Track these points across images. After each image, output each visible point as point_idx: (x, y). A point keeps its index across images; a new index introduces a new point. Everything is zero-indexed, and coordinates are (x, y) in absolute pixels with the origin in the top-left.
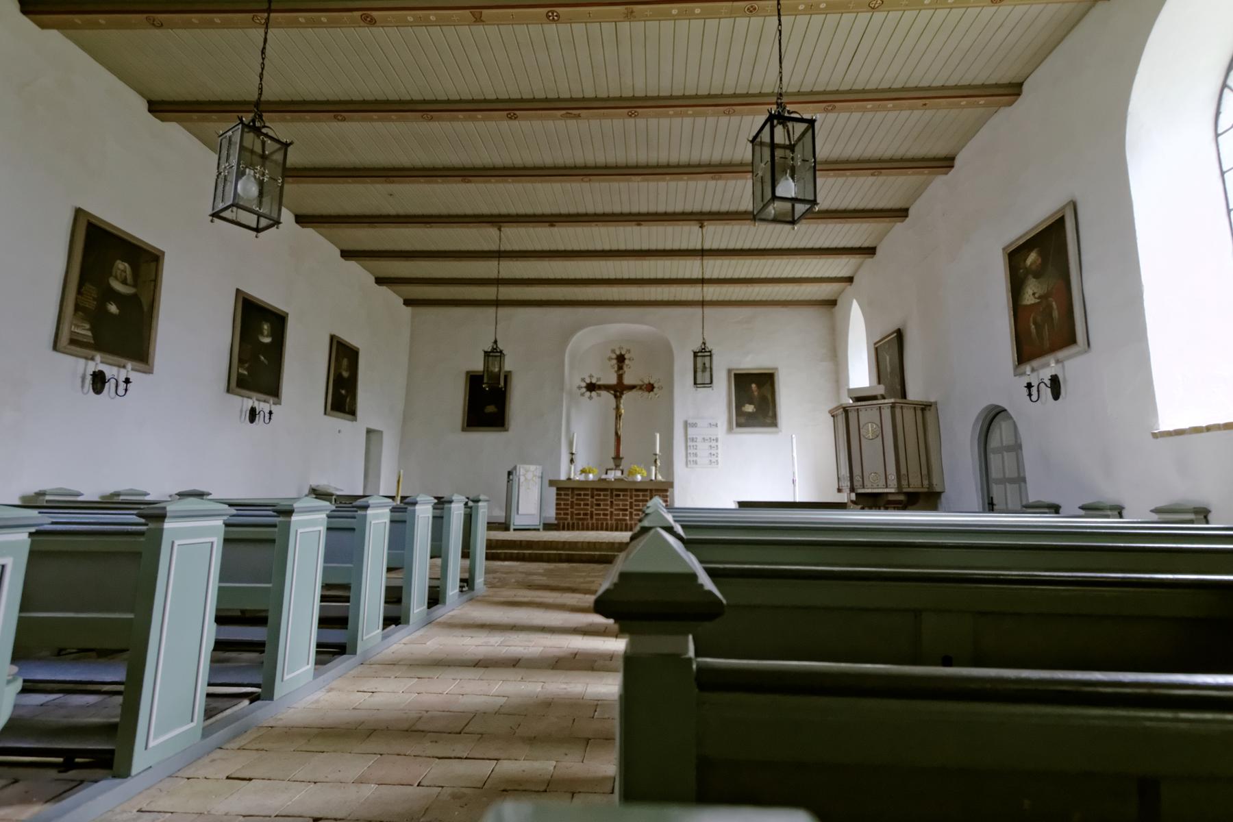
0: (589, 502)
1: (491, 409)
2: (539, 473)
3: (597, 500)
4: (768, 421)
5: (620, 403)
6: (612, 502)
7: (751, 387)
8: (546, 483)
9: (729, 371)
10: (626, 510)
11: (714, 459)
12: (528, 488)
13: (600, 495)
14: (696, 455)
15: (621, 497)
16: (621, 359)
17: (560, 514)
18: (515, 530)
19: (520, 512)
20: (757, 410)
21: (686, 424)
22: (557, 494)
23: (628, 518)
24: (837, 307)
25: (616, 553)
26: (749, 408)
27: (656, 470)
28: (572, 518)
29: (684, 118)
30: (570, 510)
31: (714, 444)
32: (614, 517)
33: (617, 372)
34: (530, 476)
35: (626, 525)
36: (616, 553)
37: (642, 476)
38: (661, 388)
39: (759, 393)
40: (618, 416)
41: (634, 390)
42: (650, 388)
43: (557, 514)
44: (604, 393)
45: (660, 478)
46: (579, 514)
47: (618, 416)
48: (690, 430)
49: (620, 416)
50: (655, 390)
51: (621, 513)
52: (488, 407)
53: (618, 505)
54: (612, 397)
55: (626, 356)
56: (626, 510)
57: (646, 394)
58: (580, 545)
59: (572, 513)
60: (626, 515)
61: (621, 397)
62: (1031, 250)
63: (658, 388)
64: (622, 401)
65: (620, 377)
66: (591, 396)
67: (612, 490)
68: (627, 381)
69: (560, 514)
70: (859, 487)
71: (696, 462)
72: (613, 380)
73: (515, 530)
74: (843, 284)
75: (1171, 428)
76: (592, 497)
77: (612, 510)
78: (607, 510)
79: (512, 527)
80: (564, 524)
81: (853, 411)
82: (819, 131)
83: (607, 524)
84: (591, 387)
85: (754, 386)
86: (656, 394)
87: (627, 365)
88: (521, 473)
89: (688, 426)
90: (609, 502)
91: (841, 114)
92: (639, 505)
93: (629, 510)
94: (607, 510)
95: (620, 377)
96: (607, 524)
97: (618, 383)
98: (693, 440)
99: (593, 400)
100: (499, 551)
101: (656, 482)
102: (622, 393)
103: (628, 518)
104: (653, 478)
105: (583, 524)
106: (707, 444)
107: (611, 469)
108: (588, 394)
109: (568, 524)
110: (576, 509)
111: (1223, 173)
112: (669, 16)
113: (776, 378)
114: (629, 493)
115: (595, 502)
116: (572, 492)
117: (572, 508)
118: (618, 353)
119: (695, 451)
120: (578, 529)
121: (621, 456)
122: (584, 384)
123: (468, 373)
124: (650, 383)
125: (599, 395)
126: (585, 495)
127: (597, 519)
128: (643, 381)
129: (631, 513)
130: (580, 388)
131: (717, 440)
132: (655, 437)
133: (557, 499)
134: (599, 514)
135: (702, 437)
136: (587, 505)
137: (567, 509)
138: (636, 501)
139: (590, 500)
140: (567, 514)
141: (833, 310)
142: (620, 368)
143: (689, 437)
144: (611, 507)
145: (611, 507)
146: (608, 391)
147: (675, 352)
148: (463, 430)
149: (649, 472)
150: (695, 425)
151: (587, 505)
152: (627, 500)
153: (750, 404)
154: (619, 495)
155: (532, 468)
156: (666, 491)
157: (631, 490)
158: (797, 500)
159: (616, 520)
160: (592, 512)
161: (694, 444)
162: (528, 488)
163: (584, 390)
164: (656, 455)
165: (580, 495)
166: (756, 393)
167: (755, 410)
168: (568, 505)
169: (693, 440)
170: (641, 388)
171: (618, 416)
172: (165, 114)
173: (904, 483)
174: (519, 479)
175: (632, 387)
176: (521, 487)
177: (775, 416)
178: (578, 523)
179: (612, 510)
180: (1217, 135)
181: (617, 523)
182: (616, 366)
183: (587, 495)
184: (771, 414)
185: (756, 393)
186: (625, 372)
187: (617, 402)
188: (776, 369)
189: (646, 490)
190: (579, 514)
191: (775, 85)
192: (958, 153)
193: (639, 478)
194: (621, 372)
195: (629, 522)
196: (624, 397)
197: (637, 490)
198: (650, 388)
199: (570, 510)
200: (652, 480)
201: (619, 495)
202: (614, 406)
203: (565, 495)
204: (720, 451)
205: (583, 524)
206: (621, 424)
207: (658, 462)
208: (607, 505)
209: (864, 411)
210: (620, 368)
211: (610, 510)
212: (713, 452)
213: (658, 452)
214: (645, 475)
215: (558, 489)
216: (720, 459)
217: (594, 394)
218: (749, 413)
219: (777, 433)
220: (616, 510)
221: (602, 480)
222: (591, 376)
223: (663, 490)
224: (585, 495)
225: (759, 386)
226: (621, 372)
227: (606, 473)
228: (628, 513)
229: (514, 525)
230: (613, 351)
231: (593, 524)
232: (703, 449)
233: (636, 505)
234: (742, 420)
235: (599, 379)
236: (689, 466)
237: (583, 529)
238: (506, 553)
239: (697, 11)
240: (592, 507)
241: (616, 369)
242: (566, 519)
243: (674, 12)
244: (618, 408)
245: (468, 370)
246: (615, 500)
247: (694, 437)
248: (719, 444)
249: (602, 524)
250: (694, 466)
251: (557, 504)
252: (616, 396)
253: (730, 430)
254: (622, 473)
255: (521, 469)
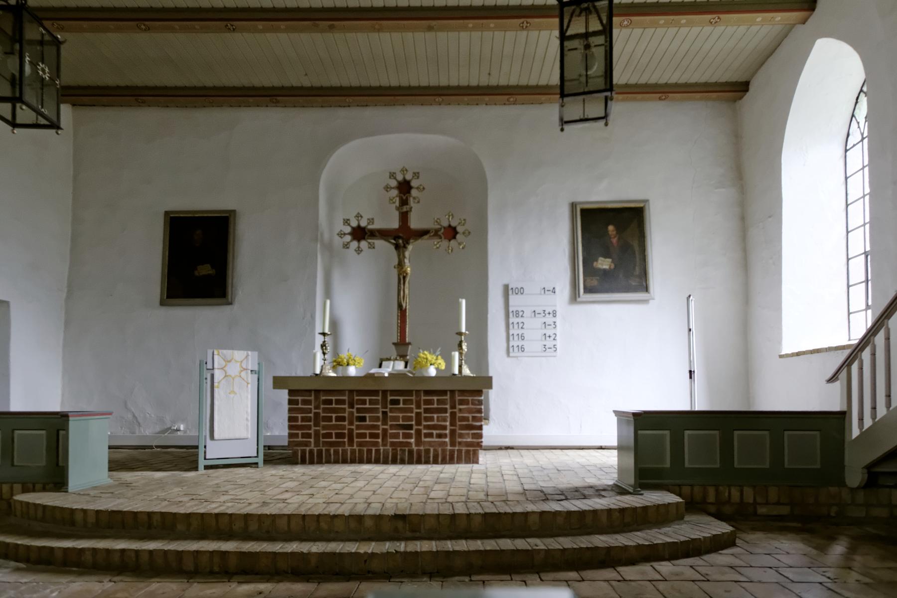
0: (346, 415)
1: (205, 270)
2: (252, 364)
3: (359, 410)
4: (634, 283)
5: (404, 257)
6: (385, 413)
7: (607, 231)
8: (268, 383)
9: (573, 206)
10: (410, 427)
11: (549, 343)
12: (233, 392)
13: (364, 402)
14: (522, 337)
15: (401, 405)
16: (405, 187)
17: (296, 435)
18: (207, 467)
19: (216, 436)
20: (616, 266)
21: (506, 289)
22: (290, 402)
23: (413, 440)
26: (604, 264)
27: (460, 360)
28: (317, 444)
29: (484, 32)
30: (313, 428)
31: (549, 319)
32: (390, 440)
33: (397, 209)
34: (233, 369)
35: (411, 452)
37: (437, 369)
38: (467, 233)
39: (619, 239)
40: (402, 277)
41: (426, 237)
42: (451, 233)
43: (291, 435)
44: (379, 243)
45: (466, 371)
46: (329, 435)
47: (402, 277)
48: (513, 299)
49: (404, 278)
50: (458, 236)
51: (401, 432)
52: (200, 267)
53: (396, 419)
54: (393, 247)
55: (414, 183)
56: (410, 427)
57: (445, 243)
58: (282, 524)
59: (317, 433)
60: (409, 436)
61: (405, 247)
63: (464, 233)
64: (407, 254)
65: (404, 217)
66: (359, 247)
67: (385, 392)
68: (415, 223)
69: (296, 435)
71: (522, 349)
72: (395, 224)
73: (207, 467)
75: (789, 352)
76: (351, 406)
77: (385, 427)
78: (377, 427)
79: (202, 463)
80: (304, 452)
82: (616, 42)
83: (378, 451)
84: (360, 234)
85: (611, 228)
86: (460, 244)
87: (414, 198)
88: (216, 366)
89: (510, 292)
90: (380, 415)
91: (635, 30)
92: (432, 419)
93: (415, 427)
94: (377, 427)
95: (404, 217)
96: (378, 451)
97: (400, 226)
98: (517, 314)
99: (363, 254)
100: (299, 455)
101: (461, 377)
102: (406, 242)
103: (413, 440)
104: (456, 371)
105: (336, 452)
106: (539, 321)
107: (389, 359)
108: (355, 244)
109: (311, 452)
110: (324, 428)
112: (465, 28)
114: (448, 397)
115: (356, 415)
116: (317, 398)
117: (316, 425)
118: (400, 177)
119: (520, 332)
120: (328, 462)
121: (407, 340)
122: (348, 229)
123: (167, 213)
124: (450, 226)
125: (372, 246)
126: (338, 402)
127: (360, 444)
128: (439, 224)
129: (418, 432)
130: (341, 234)
131: (554, 314)
132: (459, 306)
133: (290, 410)
134: (363, 436)
135: (533, 309)
136: (343, 419)
137: (309, 428)
138: (427, 411)
139: (348, 410)
140: (309, 436)
142: (404, 202)
143: (511, 309)
144: (385, 422)
145: (385, 422)
146: (386, 240)
147: (489, 186)
148: (162, 303)
149: (449, 361)
150: (520, 291)
151: (343, 419)
152: (411, 410)
153: (606, 257)
154: (396, 402)
155: (239, 355)
156: (479, 392)
157: (418, 392)
159: (392, 444)
160: (351, 432)
161: (520, 320)
162: (233, 392)
163: (348, 238)
164: (460, 334)
165: (330, 402)
166: (615, 241)
167: (613, 266)
168: (309, 419)
169: (517, 314)
170: (436, 234)
171: (402, 277)
172: (82, 98)
174: (212, 376)
175: (422, 234)
176: (216, 390)
177: (644, 274)
178: (328, 451)
179: (385, 427)
181: (394, 450)
182: (398, 199)
183: (342, 402)
184: (637, 271)
185: (615, 241)
186: (411, 208)
187: (399, 256)
188: (646, 201)
189: (444, 393)
190: (329, 435)
191: (556, 56)
193: (432, 372)
194: (405, 209)
195: (414, 448)
196: (410, 247)
197: (428, 392)
198: (451, 233)
199: (313, 428)
200: (454, 375)
201: (396, 402)
202: (396, 262)
203: (305, 402)
204: (558, 331)
205: (336, 452)
206: (407, 291)
207: (464, 347)
208: (377, 419)
210: (404, 202)
211: (415, 411)
212: (549, 332)
213: (463, 330)
214: (443, 367)
215: (291, 392)
216: (558, 343)
217: (364, 244)
218: (605, 270)
219: (646, 301)
220: (392, 427)
221: (370, 377)
222: (359, 216)
224: (338, 402)
225: (620, 230)
226: (405, 209)
227: (380, 366)
228: (413, 432)
229: (205, 459)
230: (392, 175)
231: (353, 452)
232: (533, 328)
233: (426, 419)
234: (594, 282)
235: (371, 221)
236: (511, 354)
237: (336, 462)
238: (94, 551)
239: (492, 25)
240: (351, 423)
241: (397, 204)
242: (307, 444)
243: (471, 25)
244: (401, 265)
245: (167, 210)
246: (391, 410)
247: (520, 309)
248: (558, 320)
249: (369, 451)
250: (521, 354)
251: (291, 419)
252: (397, 247)
253: (574, 298)
254: (406, 367)
255: (216, 357)
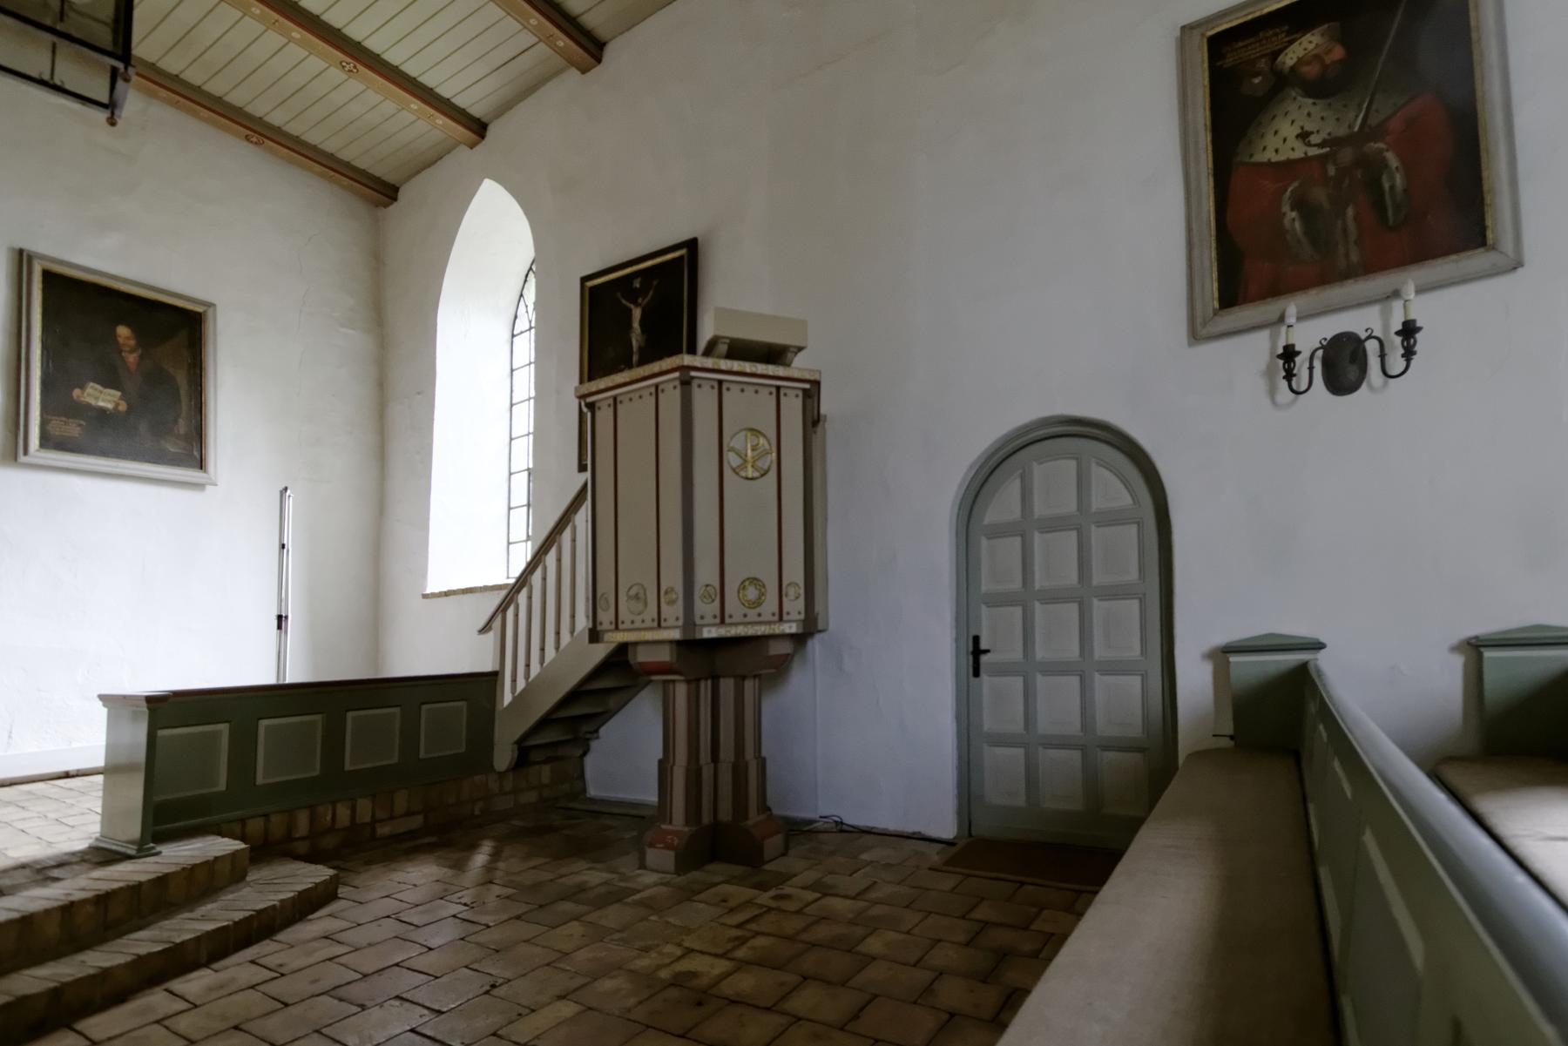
7: (114, 336)
24: (394, 207)
25: (49, 417)
36: (49, 417)
62: (637, 277)
70: (709, 620)
74: (460, 128)
81: (706, 387)
111: (512, 370)
113: (209, 328)
141: (382, 212)
158: (288, 681)
173: (705, 608)
180: (513, 336)
184: (182, 427)
188: (210, 305)
192: (611, 40)
209: (735, 389)
219: (199, 486)
223: (1284, 63)
234: (73, 429)
